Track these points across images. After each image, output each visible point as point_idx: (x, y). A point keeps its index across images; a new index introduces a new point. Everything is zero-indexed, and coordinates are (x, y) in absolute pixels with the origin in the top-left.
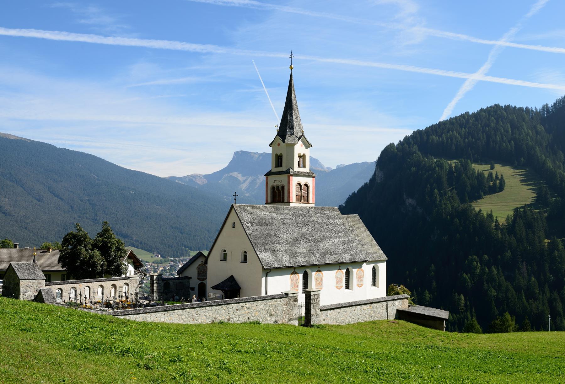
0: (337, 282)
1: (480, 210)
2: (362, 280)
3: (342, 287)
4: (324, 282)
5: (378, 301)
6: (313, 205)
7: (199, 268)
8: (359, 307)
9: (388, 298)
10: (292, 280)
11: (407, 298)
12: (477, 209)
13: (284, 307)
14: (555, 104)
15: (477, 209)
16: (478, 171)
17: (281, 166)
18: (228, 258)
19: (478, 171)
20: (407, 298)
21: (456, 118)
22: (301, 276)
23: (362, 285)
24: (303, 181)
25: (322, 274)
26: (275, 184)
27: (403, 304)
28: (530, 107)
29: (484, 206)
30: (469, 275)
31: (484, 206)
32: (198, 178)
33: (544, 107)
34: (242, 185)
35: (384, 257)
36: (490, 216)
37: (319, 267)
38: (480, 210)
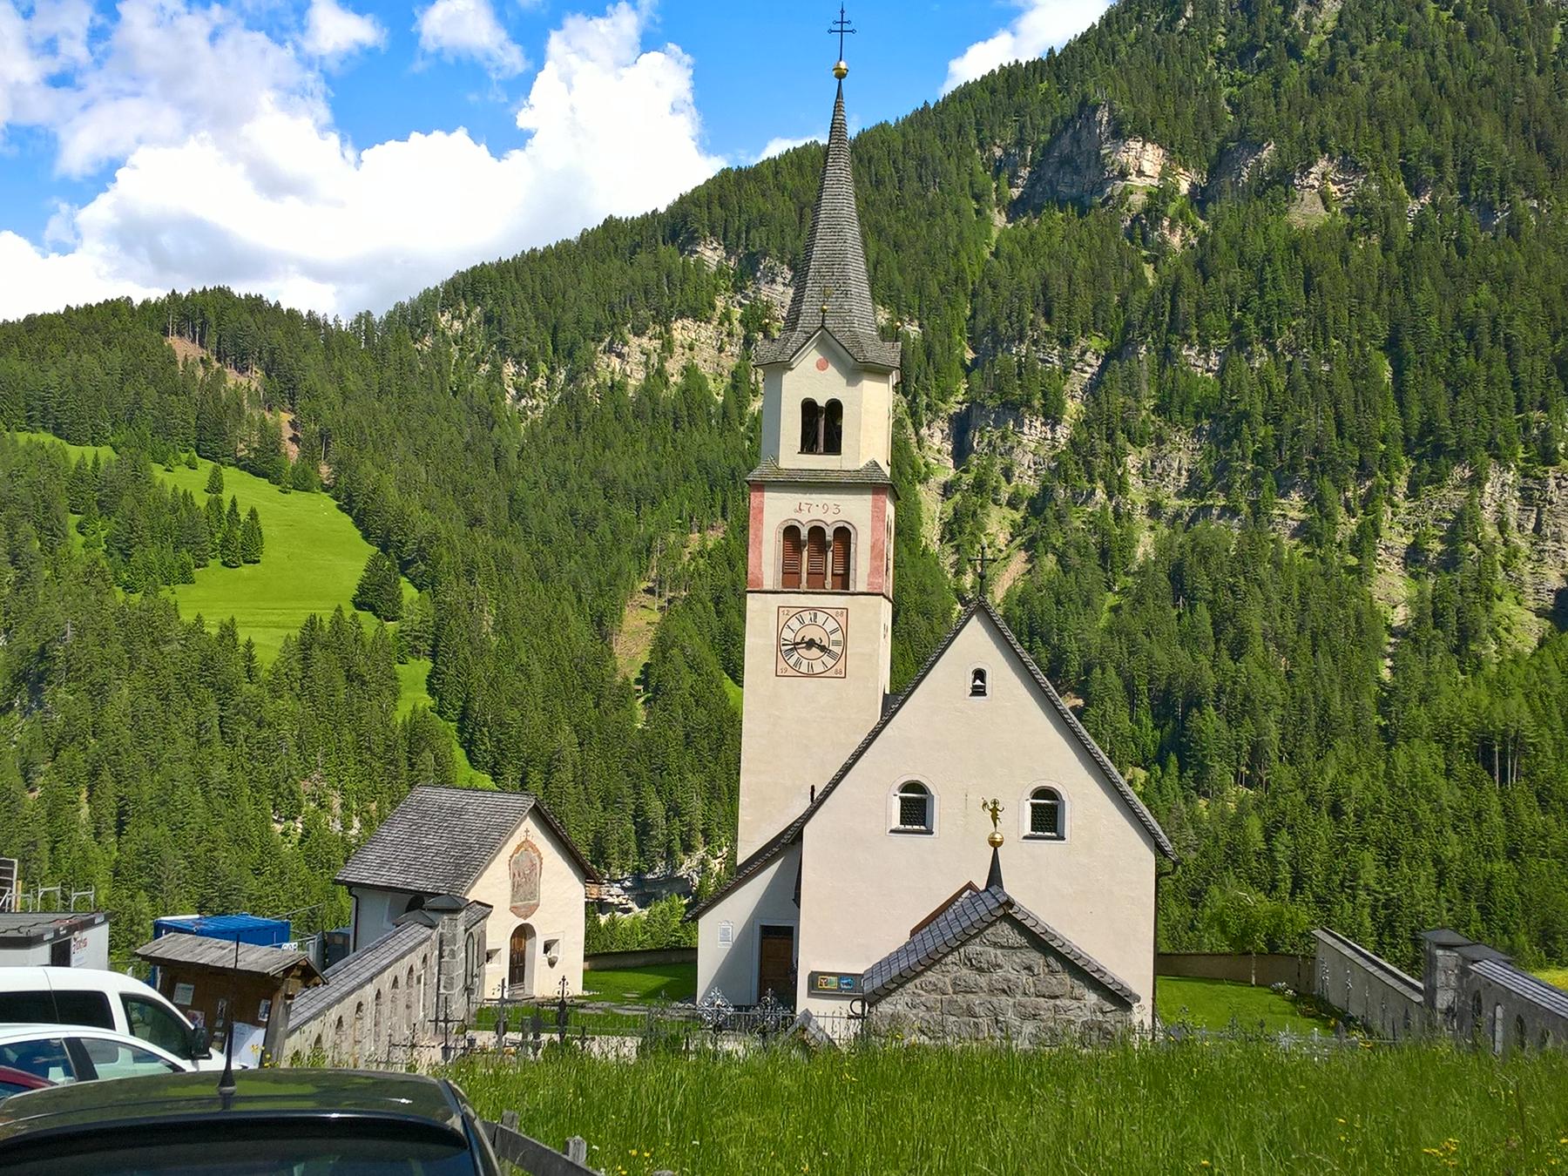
1: (199, 619)
7: (513, 862)
12: (187, 617)
14: (391, 315)
15: (187, 617)
16: (175, 488)
17: (833, 447)
21: (88, 308)
26: (805, 521)
28: (319, 313)
29: (208, 600)
31: (208, 600)
33: (358, 321)
36: (228, 631)
38: (199, 619)
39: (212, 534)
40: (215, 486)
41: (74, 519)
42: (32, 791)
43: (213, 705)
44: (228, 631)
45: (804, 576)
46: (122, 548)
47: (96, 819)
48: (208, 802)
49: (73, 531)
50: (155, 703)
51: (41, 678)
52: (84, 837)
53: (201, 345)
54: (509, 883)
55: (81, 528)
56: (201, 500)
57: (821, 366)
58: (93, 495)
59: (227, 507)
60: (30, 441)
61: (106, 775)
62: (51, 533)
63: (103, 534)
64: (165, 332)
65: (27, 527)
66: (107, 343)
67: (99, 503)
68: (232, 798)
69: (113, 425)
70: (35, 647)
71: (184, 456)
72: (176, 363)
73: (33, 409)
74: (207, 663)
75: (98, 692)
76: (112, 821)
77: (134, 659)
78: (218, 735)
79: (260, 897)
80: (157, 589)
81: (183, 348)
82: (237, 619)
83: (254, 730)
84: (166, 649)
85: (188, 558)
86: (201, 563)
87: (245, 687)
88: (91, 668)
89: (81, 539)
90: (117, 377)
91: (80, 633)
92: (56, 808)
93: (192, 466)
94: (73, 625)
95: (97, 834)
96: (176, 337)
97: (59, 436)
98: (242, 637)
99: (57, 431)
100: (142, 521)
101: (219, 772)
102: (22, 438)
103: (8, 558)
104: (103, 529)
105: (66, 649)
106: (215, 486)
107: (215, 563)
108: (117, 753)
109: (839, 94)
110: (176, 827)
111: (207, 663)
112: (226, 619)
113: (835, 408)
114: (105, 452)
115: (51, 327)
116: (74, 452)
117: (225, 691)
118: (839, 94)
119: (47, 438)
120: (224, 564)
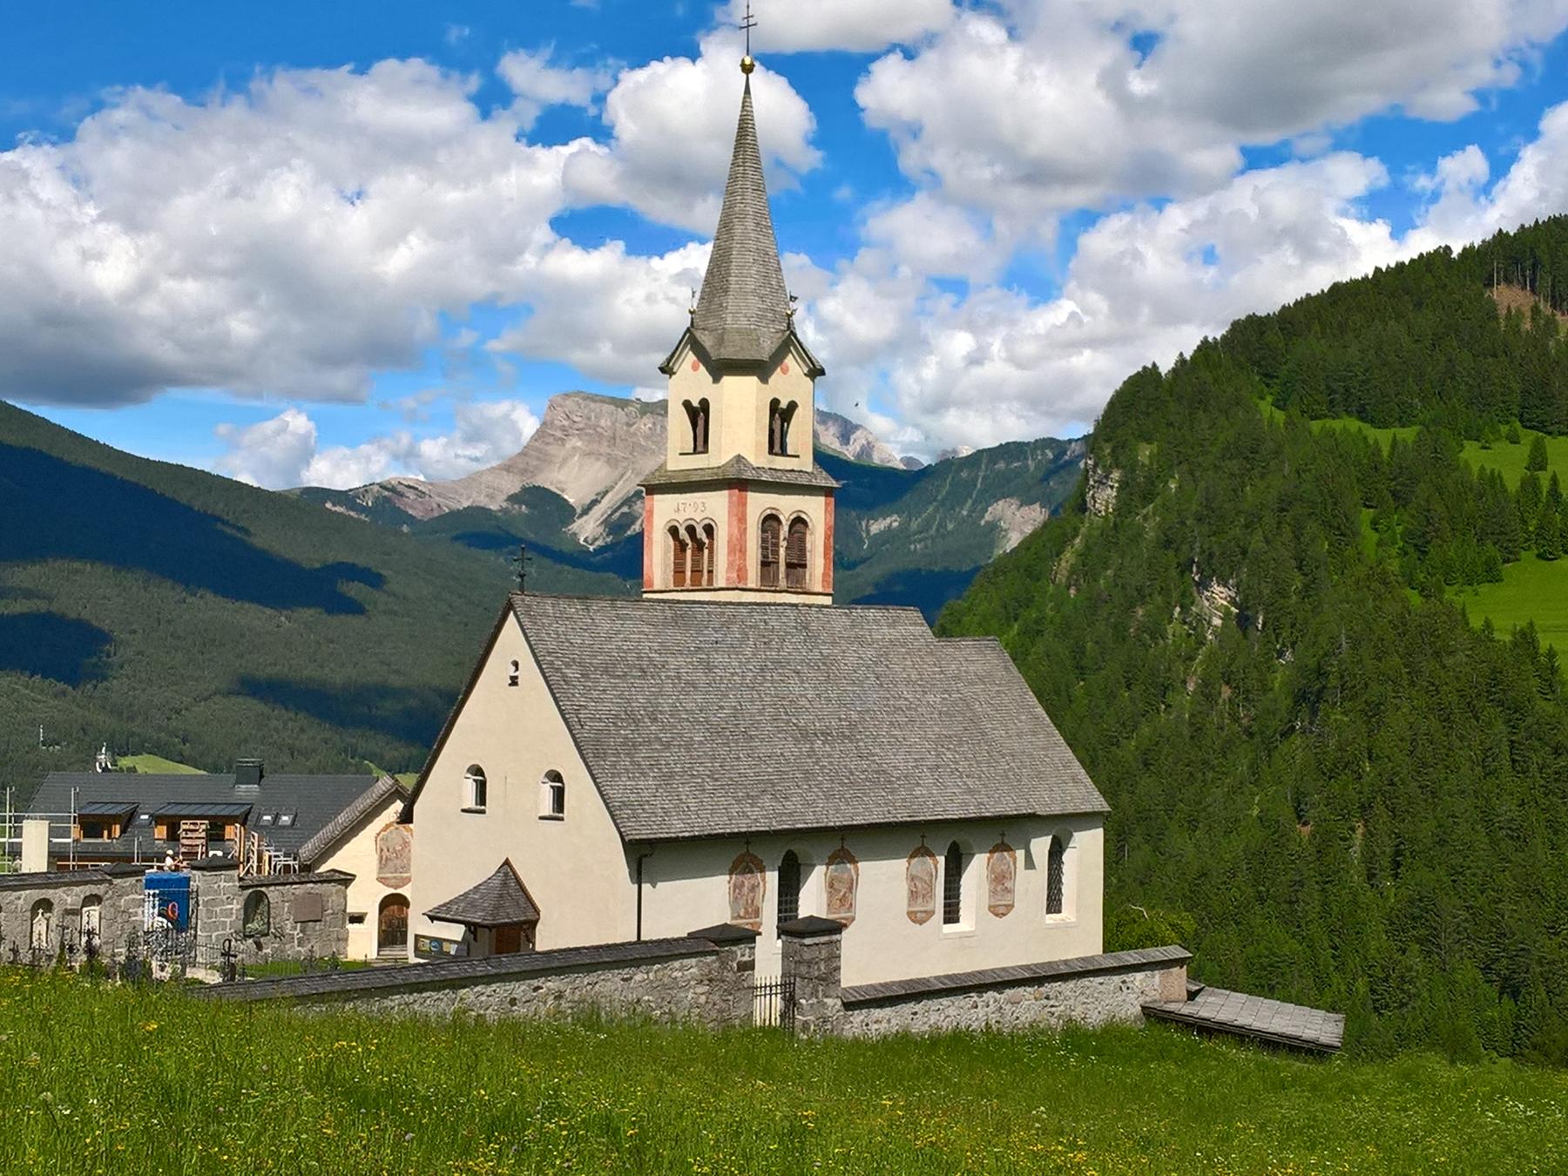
0: (913, 895)
1: (1488, 625)
2: (1009, 891)
3: (931, 913)
4: (862, 896)
5: (1064, 969)
6: (828, 601)
8: (990, 995)
9: (1110, 962)
10: (737, 887)
11: (1179, 962)
12: (1476, 623)
13: (700, 990)
15: (1476, 623)
16: (1482, 468)
18: (1151, 20)
19: (1482, 468)
20: (1179, 962)
22: (772, 878)
23: (1010, 907)
24: (787, 505)
25: (857, 870)
26: (681, 519)
27: (1164, 988)
30: (21, 135)
32: (411, 495)
34: (579, 522)
35: (1086, 795)
36: (1526, 639)
37: (848, 843)
38: (1488, 625)
39: (1525, 522)
40: (1538, 461)
41: (1367, 515)
42: (1305, 824)
43: (1500, 727)
44: (1526, 639)
45: (688, 573)
46: (1419, 545)
47: (1369, 858)
48: (1494, 843)
49: (1366, 529)
50: (1434, 724)
51: (1319, 695)
52: (1357, 878)
53: (1533, 291)
54: (376, 857)
55: (1374, 524)
56: (1512, 482)
57: (695, 368)
58: (1390, 486)
59: (1545, 485)
60: (1360, 430)
61: (1379, 808)
62: (1343, 532)
63: (1399, 529)
64: (1489, 284)
65: (1312, 527)
66: (1419, 305)
67: (1394, 494)
68: (1520, 837)
69: (1422, 401)
70: (1312, 663)
71: (1504, 429)
72: (1496, 318)
73: (1334, 392)
74: (1495, 677)
75: (1373, 713)
76: (1386, 862)
77: (1414, 672)
78: (1507, 764)
79: (1554, 962)
80: (1442, 591)
81: (1508, 297)
82: (1538, 623)
83: (1550, 759)
84: (1449, 661)
85: (1491, 549)
86: (1510, 556)
87: (1541, 704)
88: (1366, 684)
89: (1375, 537)
90: (1428, 343)
91: (1355, 644)
92: (1325, 844)
93: (1514, 441)
94: (1348, 637)
95: (1371, 876)
96: (1502, 286)
97: (1363, 419)
98: (1544, 644)
99: (1362, 415)
100: (1439, 509)
101: (1507, 808)
102: (1316, 426)
103: (1294, 563)
104: (1399, 524)
105: (1340, 663)
106: (1538, 461)
107: (1528, 556)
108: (1392, 784)
109: (747, 91)
110: (1455, 872)
111: (1495, 677)
112: (1522, 624)
113: (705, 404)
114: (1408, 434)
115: (1357, 295)
116: (1382, 437)
117: (1515, 711)
118: (747, 91)
119: (1353, 424)
120: (1540, 556)
